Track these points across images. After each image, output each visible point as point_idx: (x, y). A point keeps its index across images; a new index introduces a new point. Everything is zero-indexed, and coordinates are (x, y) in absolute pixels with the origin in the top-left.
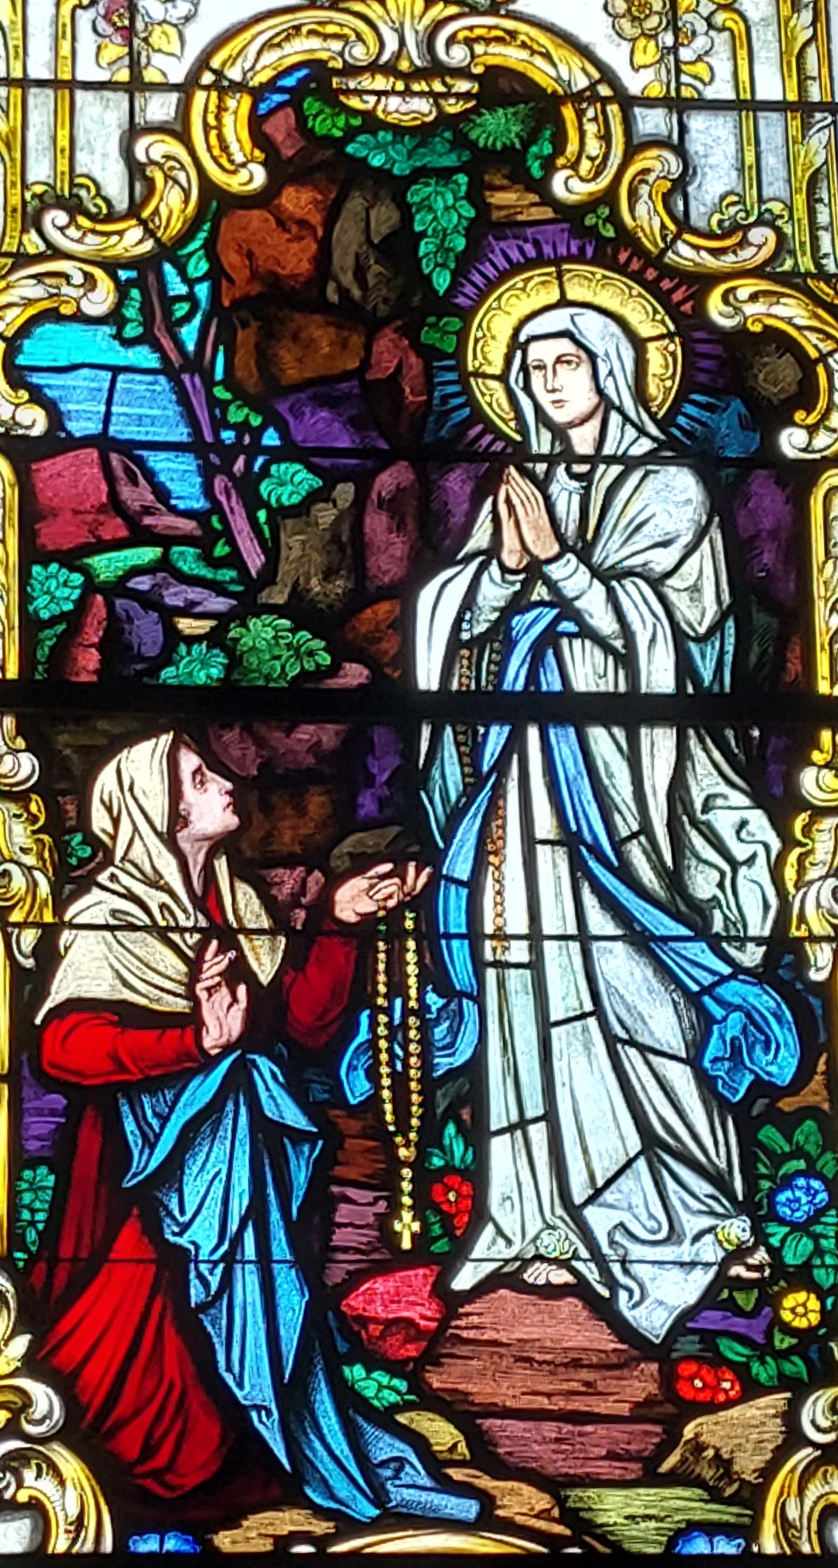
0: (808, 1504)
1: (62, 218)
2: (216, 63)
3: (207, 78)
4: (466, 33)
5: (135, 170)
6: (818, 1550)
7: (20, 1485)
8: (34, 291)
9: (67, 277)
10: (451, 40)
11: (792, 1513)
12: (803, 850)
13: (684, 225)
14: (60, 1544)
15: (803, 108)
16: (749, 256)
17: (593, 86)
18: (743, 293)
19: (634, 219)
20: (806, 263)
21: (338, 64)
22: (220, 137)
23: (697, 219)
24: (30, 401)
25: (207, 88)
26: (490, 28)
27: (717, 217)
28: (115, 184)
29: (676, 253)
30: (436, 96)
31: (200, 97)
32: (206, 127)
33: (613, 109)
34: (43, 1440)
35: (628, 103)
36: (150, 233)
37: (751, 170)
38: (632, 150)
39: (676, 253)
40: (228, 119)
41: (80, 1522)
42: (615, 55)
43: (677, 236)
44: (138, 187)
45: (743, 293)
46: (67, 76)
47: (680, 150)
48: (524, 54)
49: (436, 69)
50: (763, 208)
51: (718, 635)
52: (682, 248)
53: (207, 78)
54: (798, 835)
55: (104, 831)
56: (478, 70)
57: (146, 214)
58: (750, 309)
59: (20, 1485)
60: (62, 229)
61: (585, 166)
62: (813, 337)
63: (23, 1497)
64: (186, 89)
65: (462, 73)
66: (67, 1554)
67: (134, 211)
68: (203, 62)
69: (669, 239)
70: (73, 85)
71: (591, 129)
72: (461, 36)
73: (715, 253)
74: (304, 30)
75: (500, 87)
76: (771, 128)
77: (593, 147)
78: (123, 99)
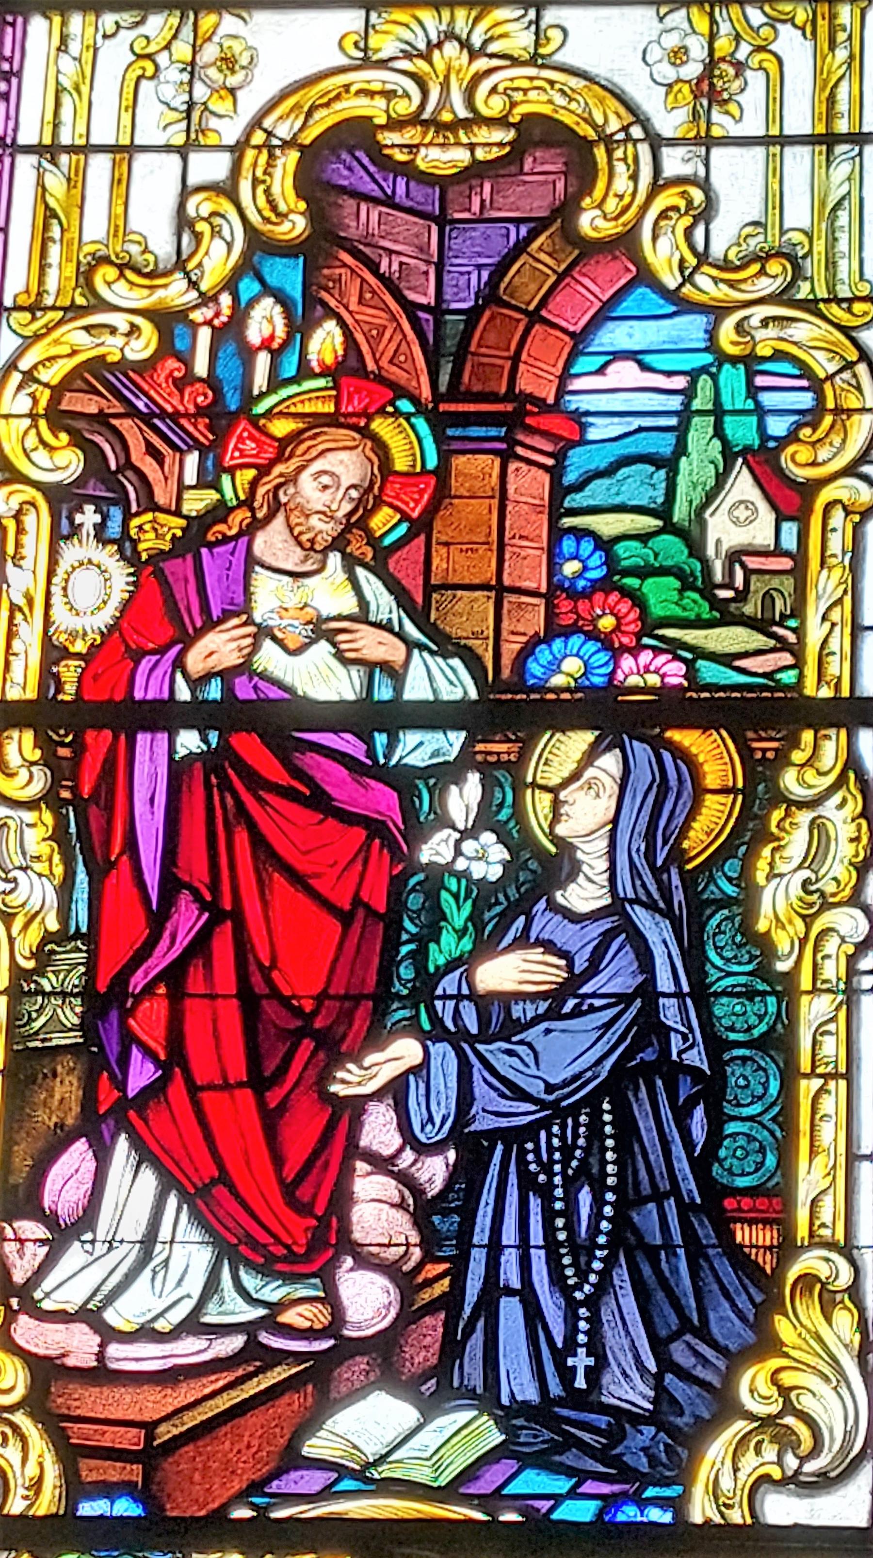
1: (111, 273)
2: (267, 123)
3: (259, 138)
4: (508, 84)
5: (183, 222)
8: (81, 338)
9: (113, 330)
12: (775, 844)
13: (703, 258)
15: (828, 140)
17: (625, 129)
18: (755, 322)
19: (688, 1344)
21: (381, 120)
22: (267, 192)
23: (717, 250)
25: (258, 147)
26: (531, 79)
28: (163, 245)
29: (694, 286)
30: (472, 147)
31: (250, 154)
32: (256, 182)
33: (644, 150)
35: (656, 142)
36: (193, 285)
37: (775, 200)
38: (657, 187)
39: (694, 286)
40: (278, 173)
42: (651, 101)
43: (696, 269)
44: (186, 238)
45: (755, 322)
46: (126, 141)
47: (705, 185)
48: (364, 101)
49: (478, 120)
50: (785, 238)
51: (671, 309)
52: (699, 279)
53: (259, 138)
56: (515, 119)
58: (760, 334)
60: (109, 284)
61: (611, 205)
62: (821, 355)
64: (238, 150)
66: (22, 1517)
67: (180, 264)
68: (257, 123)
69: (687, 273)
71: (620, 167)
72: (501, 88)
74: (353, 89)
75: (537, 134)
76: (798, 161)
77: (622, 183)
78: (175, 160)
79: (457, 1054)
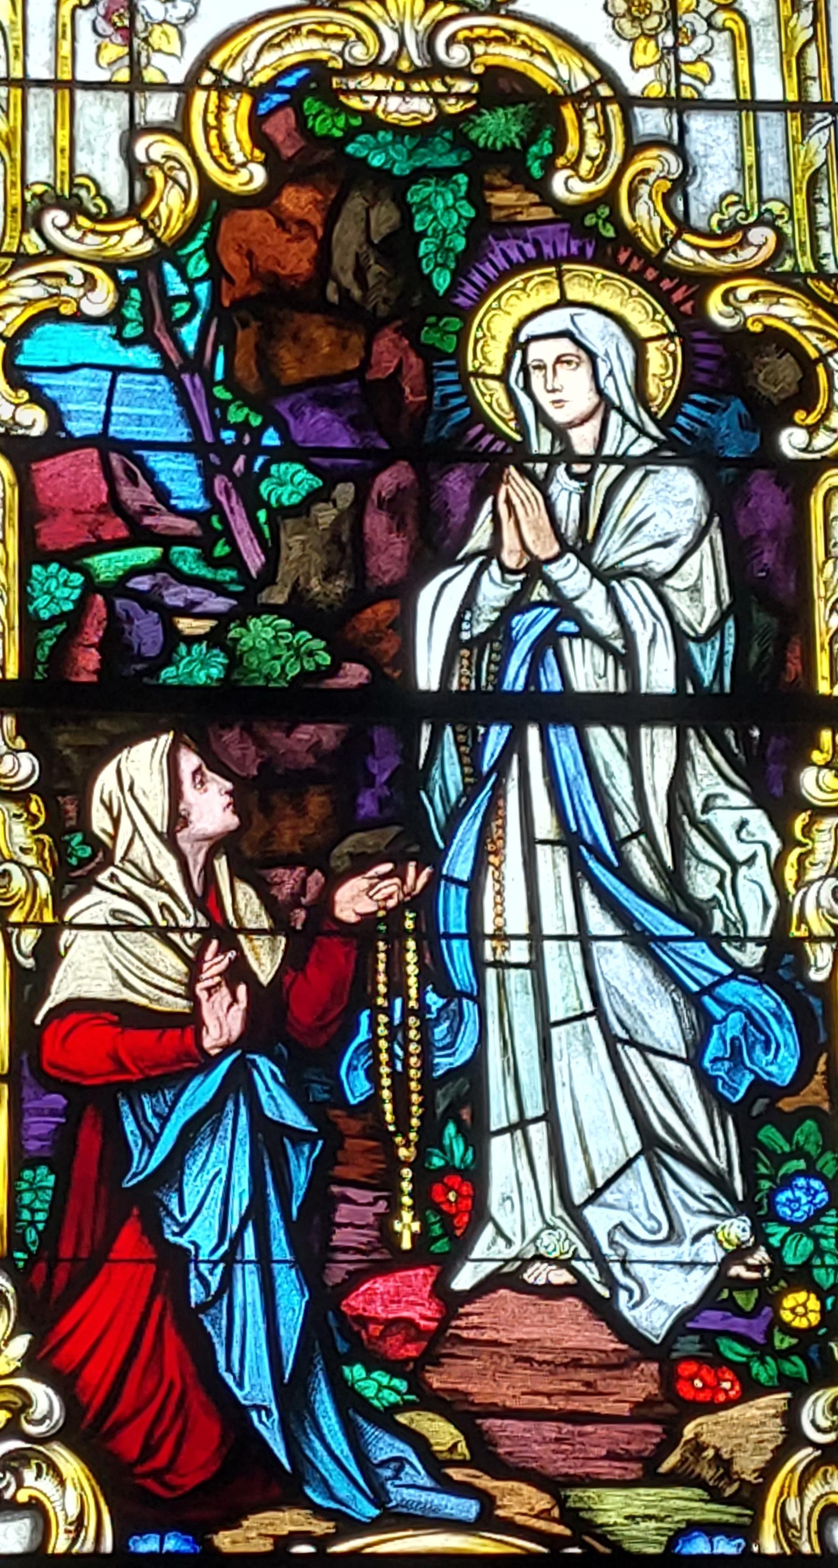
0: (808, 1504)
1: (62, 218)
2: (216, 63)
3: (207, 78)
4: (466, 33)
5: (135, 170)
6: (818, 1550)
7: (20, 1485)
8: (34, 291)
9: (67, 277)
10: (451, 40)
11: (792, 1513)
12: (803, 850)
13: (684, 225)
14: (60, 1544)
15: (803, 108)
16: (749, 256)
17: (593, 86)
18: (743, 293)
20: (806, 263)
21: (338, 64)
22: (220, 137)
23: (697, 219)
24: (30, 401)
25: (207, 88)
26: (490, 28)
27: (717, 217)
28: (115, 184)
29: (676, 253)
30: (436, 96)
31: (200, 97)
32: (206, 127)
33: (613, 109)
34: (43, 1440)
35: (628, 103)
36: (150, 233)
37: (751, 170)
38: (632, 150)
39: (676, 253)
40: (228, 119)
41: (80, 1522)
42: (615, 55)
43: (677, 236)
44: (138, 187)
45: (743, 293)
46: (67, 76)
47: (680, 150)
49: (436, 69)
50: (763, 208)
51: (718, 635)
52: (682, 248)
53: (207, 78)
54: (798, 835)
56: (478, 70)
57: (146, 214)
58: (750, 309)
59: (20, 1485)
60: (62, 229)
61: (585, 166)
62: (813, 337)
63: (23, 1497)
64: (186, 89)
65: (462, 73)
67: (134, 211)
68: (203, 62)
69: (669, 239)
70: (73, 85)
71: (591, 129)
72: (461, 36)
73: (715, 253)
74: (304, 30)
75: (500, 87)
76: (771, 128)
77: (593, 147)
78: (123, 99)
79: (530, 1483)
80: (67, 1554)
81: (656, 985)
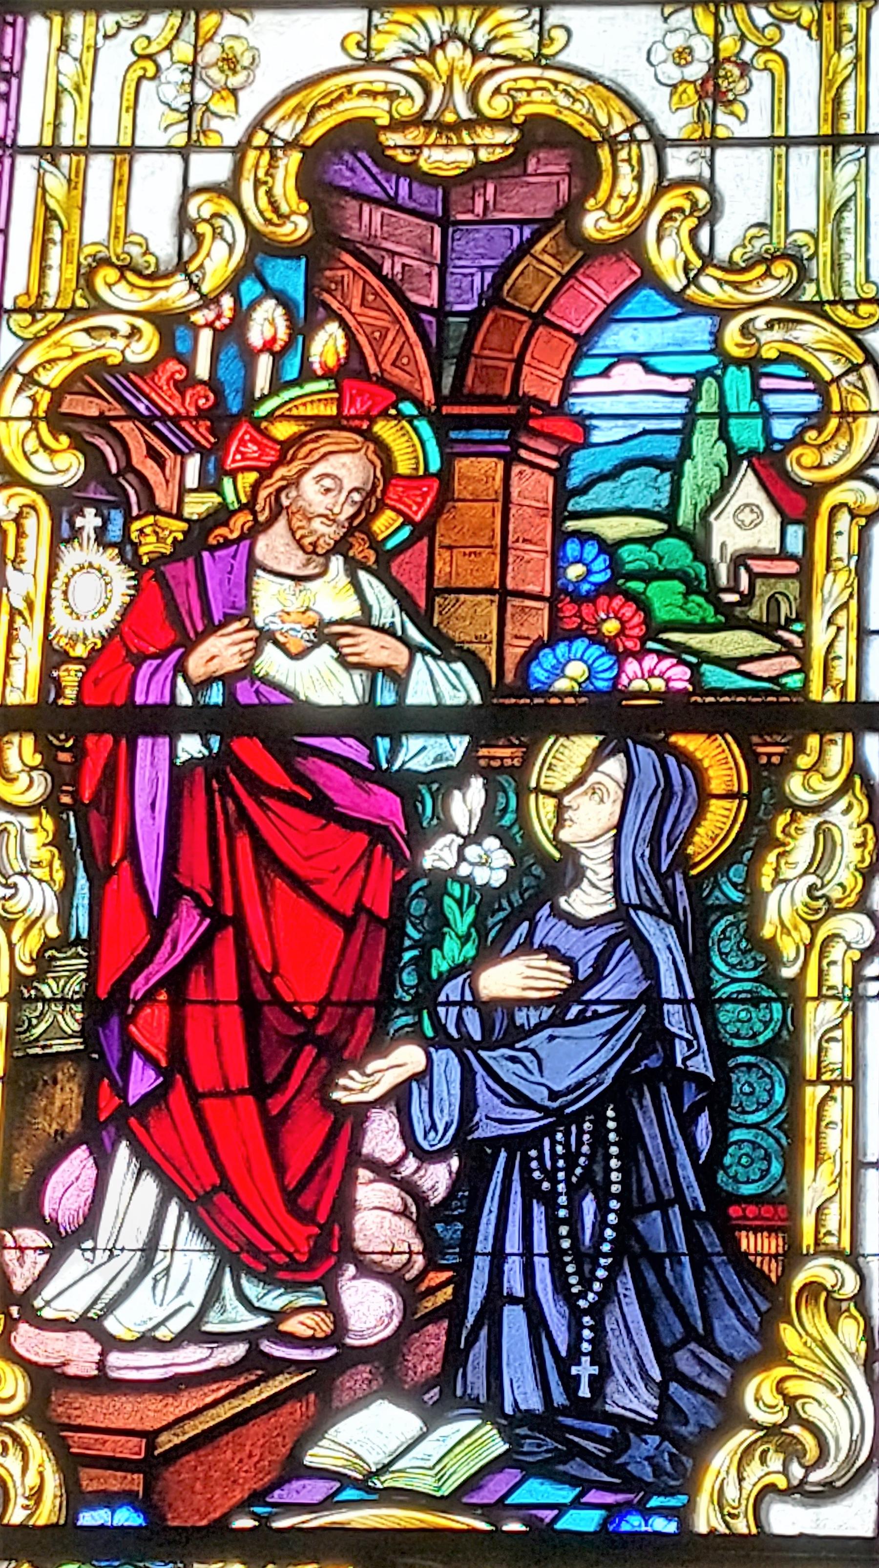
1: (112, 274)
2: (269, 124)
3: (260, 138)
4: (512, 84)
5: (184, 223)
8: (82, 341)
9: (114, 333)
12: (781, 850)
13: (708, 260)
15: (834, 141)
17: (629, 130)
18: (760, 324)
21: (384, 121)
22: (269, 193)
23: (722, 252)
25: (260, 148)
26: (535, 79)
28: (164, 247)
29: (699, 287)
30: (475, 148)
31: (252, 155)
32: (257, 183)
33: (648, 151)
35: (661, 143)
36: (195, 286)
37: (780, 202)
38: (661, 188)
39: (699, 287)
40: (280, 174)
42: (655, 102)
43: (701, 271)
44: (187, 240)
45: (760, 324)
46: (127, 142)
47: (710, 186)
49: (482, 121)
50: (790, 240)
52: (704, 281)
53: (260, 138)
55: (723, 545)
56: (518, 120)
58: (765, 337)
60: (110, 286)
61: (616, 206)
62: (826, 358)
64: (239, 151)
67: (182, 266)
68: (258, 124)
69: (692, 275)
71: (624, 168)
72: (504, 89)
74: (356, 90)
75: (540, 135)
76: (804, 162)
77: (626, 185)
78: (176, 161)
80: (22, 1526)
81: (621, 80)
